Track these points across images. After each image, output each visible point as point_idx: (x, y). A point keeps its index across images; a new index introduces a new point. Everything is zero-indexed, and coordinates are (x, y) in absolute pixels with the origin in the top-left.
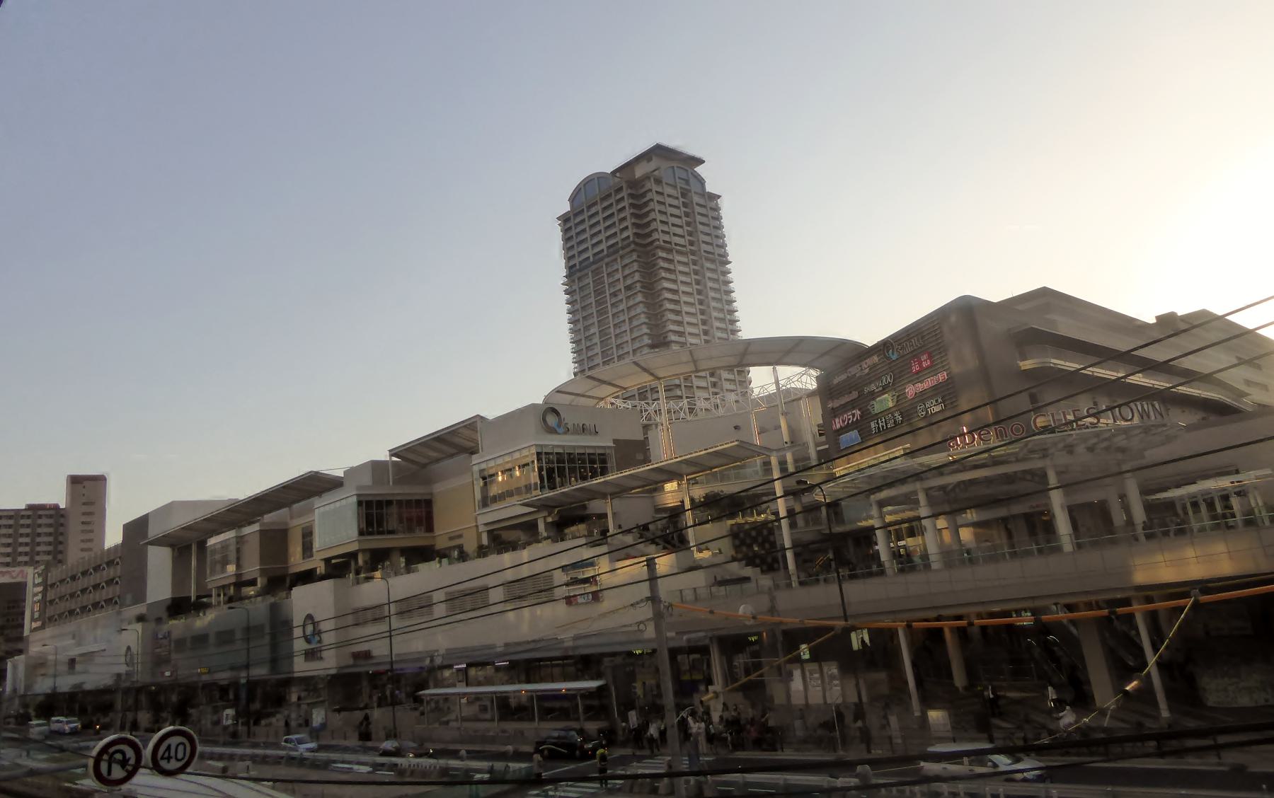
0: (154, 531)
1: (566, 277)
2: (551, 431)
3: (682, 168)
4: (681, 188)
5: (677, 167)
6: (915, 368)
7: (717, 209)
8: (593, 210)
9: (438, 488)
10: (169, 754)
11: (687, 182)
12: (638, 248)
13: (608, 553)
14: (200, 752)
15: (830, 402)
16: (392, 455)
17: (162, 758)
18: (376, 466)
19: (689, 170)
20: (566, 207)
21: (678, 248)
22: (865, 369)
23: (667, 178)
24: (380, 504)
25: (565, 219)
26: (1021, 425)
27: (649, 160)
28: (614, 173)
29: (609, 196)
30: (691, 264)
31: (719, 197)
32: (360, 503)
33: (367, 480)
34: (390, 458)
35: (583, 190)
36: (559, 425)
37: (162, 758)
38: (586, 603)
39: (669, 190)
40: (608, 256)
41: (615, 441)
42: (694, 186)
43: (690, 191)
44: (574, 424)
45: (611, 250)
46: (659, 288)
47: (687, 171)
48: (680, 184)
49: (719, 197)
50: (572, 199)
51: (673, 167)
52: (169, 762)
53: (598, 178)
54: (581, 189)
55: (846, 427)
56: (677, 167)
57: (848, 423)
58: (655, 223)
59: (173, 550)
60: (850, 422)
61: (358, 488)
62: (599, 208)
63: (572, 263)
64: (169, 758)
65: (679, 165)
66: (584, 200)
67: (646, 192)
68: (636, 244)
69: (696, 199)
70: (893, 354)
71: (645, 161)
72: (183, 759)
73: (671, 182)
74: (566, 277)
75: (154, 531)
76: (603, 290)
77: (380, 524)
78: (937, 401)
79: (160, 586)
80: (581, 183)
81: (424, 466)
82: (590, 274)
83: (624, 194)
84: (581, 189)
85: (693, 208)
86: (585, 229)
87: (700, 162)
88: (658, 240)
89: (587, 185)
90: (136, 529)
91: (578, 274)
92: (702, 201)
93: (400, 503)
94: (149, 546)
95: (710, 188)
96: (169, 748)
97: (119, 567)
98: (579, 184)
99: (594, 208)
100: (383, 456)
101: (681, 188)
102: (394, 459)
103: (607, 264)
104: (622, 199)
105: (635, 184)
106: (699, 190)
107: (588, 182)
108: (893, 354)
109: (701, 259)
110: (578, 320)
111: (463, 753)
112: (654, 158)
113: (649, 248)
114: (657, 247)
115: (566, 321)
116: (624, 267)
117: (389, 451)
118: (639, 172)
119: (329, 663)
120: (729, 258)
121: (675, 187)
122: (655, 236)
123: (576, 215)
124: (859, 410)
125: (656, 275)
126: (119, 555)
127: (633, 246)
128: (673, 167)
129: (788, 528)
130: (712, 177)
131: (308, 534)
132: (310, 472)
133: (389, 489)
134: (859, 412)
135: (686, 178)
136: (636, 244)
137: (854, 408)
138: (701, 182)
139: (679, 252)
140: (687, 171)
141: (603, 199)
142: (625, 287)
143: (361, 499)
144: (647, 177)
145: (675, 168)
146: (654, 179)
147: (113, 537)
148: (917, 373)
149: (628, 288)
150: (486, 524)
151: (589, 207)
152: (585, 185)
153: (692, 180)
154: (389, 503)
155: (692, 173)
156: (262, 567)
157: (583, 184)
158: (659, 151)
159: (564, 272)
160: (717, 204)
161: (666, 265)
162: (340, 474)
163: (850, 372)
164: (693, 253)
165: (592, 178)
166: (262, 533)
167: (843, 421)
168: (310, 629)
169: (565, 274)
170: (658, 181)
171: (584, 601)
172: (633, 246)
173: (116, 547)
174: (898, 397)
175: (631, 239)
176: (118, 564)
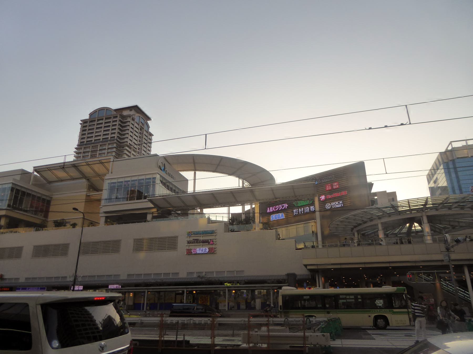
3: (143, 119)
4: (141, 126)
5: (142, 118)
6: (328, 188)
8: (100, 122)
9: (56, 196)
12: (118, 143)
14: (339, 319)
18: (24, 173)
19: (145, 121)
20: (87, 117)
23: (137, 120)
24: (24, 193)
25: (84, 122)
27: (131, 110)
28: (116, 110)
29: (110, 118)
31: (153, 135)
32: (12, 189)
35: (97, 112)
39: (136, 125)
40: (102, 142)
42: (145, 128)
45: (104, 140)
47: (144, 120)
48: (141, 124)
49: (153, 135)
50: (91, 115)
53: (106, 109)
54: (97, 111)
55: (276, 211)
56: (142, 118)
57: (278, 209)
58: (128, 135)
60: (280, 209)
65: (142, 117)
66: (97, 116)
67: (127, 122)
68: (117, 141)
69: (145, 133)
71: (129, 110)
73: (138, 122)
76: (96, 155)
78: (339, 203)
80: (98, 109)
81: (50, 182)
82: (91, 147)
83: (118, 119)
84: (97, 111)
86: (94, 128)
88: (127, 142)
91: (84, 146)
92: (147, 134)
95: (151, 130)
98: (97, 109)
99: (100, 121)
100: (30, 170)
101: (141, 126)
102: (35, 173)
103: (100, 145)
104: (116, 121)
105: (123, 117)
106: (147, 130)
107: (100, 110)
112: (133, 110)
113: (122, 144)
116: (108, 149)
117: (34, 167)
118: (125, 113)
121: (138, 125)
125: (122, 156)
127: (115, 141)
128: (140, 117)
130: (153, 127)
133: (29, 186)
136: (117, 141)
138: (148, 127)
139: (134, 150)
140: (144, 120)
141: (106, 119)
143: (14, 186)
144: (129, 116)
146: (132, 118)
150: (106, 212)
151: (98, 120)
153: (145, 125)
154: (29, 195)
155: (146, 122)
157: (99, 110)
158: (136, 108)
161: (127, 153)
165: (96, 111)
167: (275, 208)
170: (133, 120)
171: (202, 252)
172: (115, 141)
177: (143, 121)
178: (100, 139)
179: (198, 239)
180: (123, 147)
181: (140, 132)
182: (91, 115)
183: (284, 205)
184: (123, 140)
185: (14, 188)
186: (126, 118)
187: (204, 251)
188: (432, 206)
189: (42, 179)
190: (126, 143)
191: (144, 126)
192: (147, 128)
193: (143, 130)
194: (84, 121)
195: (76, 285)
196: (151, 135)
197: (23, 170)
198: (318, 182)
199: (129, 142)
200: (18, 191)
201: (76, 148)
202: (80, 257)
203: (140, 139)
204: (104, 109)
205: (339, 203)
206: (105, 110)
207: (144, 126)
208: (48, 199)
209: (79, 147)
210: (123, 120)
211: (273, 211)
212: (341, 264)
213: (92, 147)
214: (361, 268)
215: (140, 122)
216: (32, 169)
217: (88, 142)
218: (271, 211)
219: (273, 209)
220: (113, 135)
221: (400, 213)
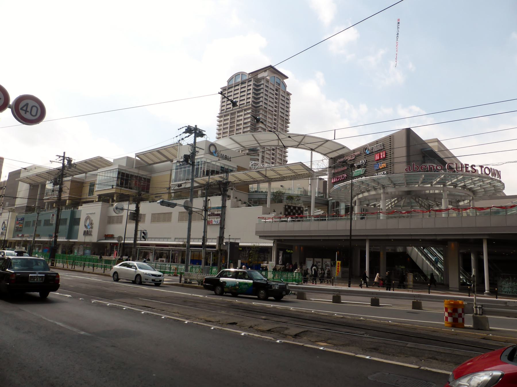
0: (23, 175)
1: (219, 114)
2: (211, 153)
7: (288, 99)
8: (237, 88)
10: (27, 108)
11: (279, 85)
12: (253, 107)
13: (199, 255)
15: (333, 170)
16: (136, 156)
17: (22, 109)
19: (281, 80)
20: (225, 84)
21: (269, 111)
22: (353, 157)
24: (127, 175)
26: (440, 166)
27: (265, 71)
28: (249, 74)
30: (273, 115)
31: (291, 94)
33: (124, 164)
34: (135, 158)
36: (215, 152)
37: (22, 109)
38: (216, 225)
41: (237, 166)
42: (282, 87)
43: (280, 89)
44: (222, 154)
46: (258, 126)
49: (291, 94)
50: (229, 81)
51: (275, 77)
52: (26, 113)
53: (242, 74)
54: (233, 77)
57: (340, 180)
59: (30, 186)
60: (341, 179)
61: (119, 166)
62: (239, 87)
63: (223, 108)
64: (26, 111)
66: (234, 83)
69: (281, 93)
70: (368, 151)
72: (35, 116)
74: (219, 114)
75: (23, 175)
77: (126, 184)
79: (21, 201)
80: (233, 75)
83: (251, 83)
85: (278, 109)
87: (287, 77)
89: (236, 77)
90: (14, 175)
93: (136, 177)
94: (20, 182)
95: (288, 90)
96: (27, 105)
97: (5, 190)
98: (233, 76)
100: (133, 156)
102: (137, 158)
108: (368, 151)
109: (278, 118)
110: (220, 134)
111: (201, 170)
114: (261, 109)
115: (216, 133)
117: (136, 154)
118: (260, 76)
119: (94, 238)
120: (290, 121)
121: (274, 85)
122: (261, 104)
123: (229, 88)
124: (346, 174)
126: (5, 185)
128: (275, 77)
129: (314, 207)
131: (92, 185)
132: (99, 156)
133: (134, 171)
134: (346, 175)
135: (279, 83)
137: (344, 174)
138: (285, 86)
142: (244, 123)
144: (263, 78)
145: (276, 77)
147: (5, 177)
148: (377, 160)
149: (245, 123)
151: (235, 86)
152: (235, 76)
153: (281, 84)
154: (132, 176)
156: (70, 196)
159: (219, 112)
160: (289, 97)
162: (112, 161)
163: (346, 158)
164: (275, 115)
166: (72, 181)
168: (88, 222)
169: (219, 113)
171: (216, 223)
173: (4, 182)
174: (366, 170)
175: (251, 103)
176: (4, 189)
177: (279, 80)
178: (244, 104)
179: (214, 213)
180: (259, 112)
181: (276, 93)
182: (229, 82)
183: (344, 175)
184: (258, 104)
185: (120, 172)
186: (260, 81)
187: (217, 222)
188: (59, 218)
189: (143, 162)
190: (261, 107)
191: (280, 86)
192: (284, 87)
193: (279, 90)
194: (224, 89)
195: (425, 249)
196: (289, 94)
197: (127, 157)
198: (370, 151)
199: (264, 105)
200: (123, 174)
201: (218, 117)
202: (192, 224)
203: (276, 100)
204: (240, 74)
205: (384, 173)
206: (241, 75)
207: (280, 86)
208: (149, 178)
209: (220, 115)
210: (258, 83)
211: (336, 181)
212: (295, 236)
213: (231, 114)
214: (392, 239)
215: (275, 83)
216: (135, 155)
217: (229, 110)
218: (335, 181)
219: (336, 179)
220: (248, 101)
221: (384, 187)
